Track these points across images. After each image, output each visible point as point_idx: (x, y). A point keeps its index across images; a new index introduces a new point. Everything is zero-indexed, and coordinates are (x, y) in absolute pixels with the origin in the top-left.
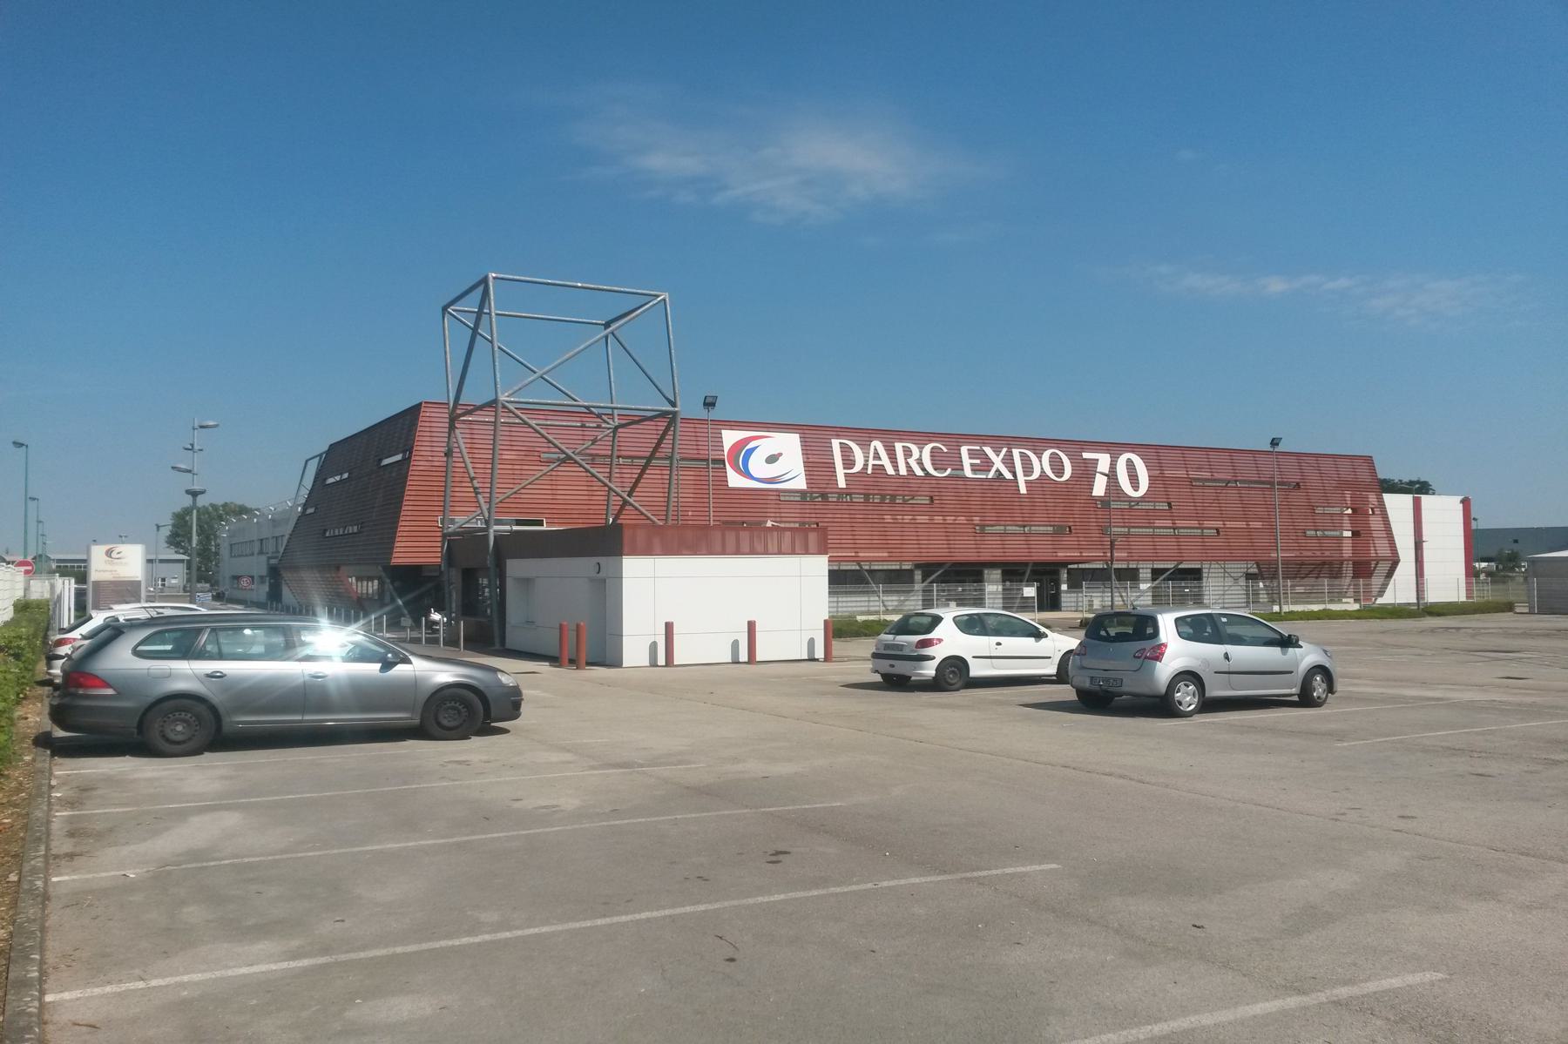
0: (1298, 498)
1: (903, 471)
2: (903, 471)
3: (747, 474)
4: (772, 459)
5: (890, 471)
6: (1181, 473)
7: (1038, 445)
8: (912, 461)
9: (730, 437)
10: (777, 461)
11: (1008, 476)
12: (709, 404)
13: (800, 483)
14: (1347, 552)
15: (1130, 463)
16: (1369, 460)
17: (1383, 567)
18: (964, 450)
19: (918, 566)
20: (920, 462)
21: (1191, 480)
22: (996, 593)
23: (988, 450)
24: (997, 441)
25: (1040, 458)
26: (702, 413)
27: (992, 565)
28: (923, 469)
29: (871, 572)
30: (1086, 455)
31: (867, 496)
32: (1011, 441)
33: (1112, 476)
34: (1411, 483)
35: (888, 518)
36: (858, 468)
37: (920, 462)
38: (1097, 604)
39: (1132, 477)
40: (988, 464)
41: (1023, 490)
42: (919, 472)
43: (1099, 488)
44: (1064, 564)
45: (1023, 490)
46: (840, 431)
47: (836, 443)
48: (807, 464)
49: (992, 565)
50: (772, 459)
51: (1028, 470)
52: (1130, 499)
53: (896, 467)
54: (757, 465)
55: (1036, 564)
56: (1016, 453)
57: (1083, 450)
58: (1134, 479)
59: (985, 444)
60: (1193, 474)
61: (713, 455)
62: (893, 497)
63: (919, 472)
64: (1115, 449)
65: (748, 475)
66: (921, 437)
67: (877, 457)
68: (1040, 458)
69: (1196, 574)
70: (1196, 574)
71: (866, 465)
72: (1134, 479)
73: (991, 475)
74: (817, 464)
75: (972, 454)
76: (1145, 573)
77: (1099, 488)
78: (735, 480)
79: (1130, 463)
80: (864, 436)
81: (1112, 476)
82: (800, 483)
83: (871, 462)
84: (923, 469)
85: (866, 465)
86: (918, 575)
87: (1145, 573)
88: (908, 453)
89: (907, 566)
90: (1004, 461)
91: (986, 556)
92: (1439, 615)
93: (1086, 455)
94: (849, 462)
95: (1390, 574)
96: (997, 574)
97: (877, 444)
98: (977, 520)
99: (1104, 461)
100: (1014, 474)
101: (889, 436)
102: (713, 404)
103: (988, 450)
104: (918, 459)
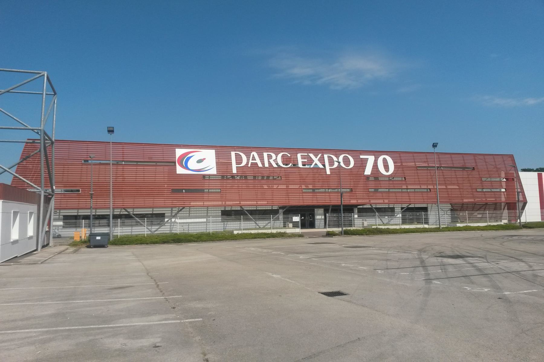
0: (475, 173)
1: (267, 165)
2: (267, 165)
3: (187, 168)
4: (200, 161)
5: (260, 165)
6: (412, 164)
7: (337, 153)
8: (272, 161)
9: (179, 152)
10: (203, 161)
11: (321, 166)
12: (435, 145)
13: (214, 171)
14: (503, 199)
15: (385, 161)
16: (511, 157)
17: (521, 205)
18: (299, 156)
19: (280, 208)
20: (275, 160)
21: (417, 168)
22: (321, 219)
23: (312, 155)
24: (316, 151)
25: (338, 158)
26: (432, 150)
27: (319, 207)
28: (277, 164)
29: (376, 208)
30: (362, 157)
31: (255, 177)
32: (324, 151)
33: (375, 166)
34: (540, 168)
35: (265, 187)
36: (244, 164)
37: (275, 160)
38: (366, 224)
39: (387, 166)
40: (311, 161)
41: (328, 172)
42: (275, 166)
43: (368, 171)
44: (356, 206)
45: (328, 172)
46: (234, 148)
47: (233, 154)
48: (217, 163)
49: (319, 207)
50: (200, 161)
51: (331, 162)
52: (389, 176)
53: (263, 164)
54: (193, 164)
55: (333, 206)
56: (326, 156)
57: (361, 154)
58: (386, 167)
59: (310, 153)
60: (418, 164)
61: (171, 160)
62: (268, 177)
63: (275, 166)
64: (377, 154)
65: (187, 168)
66: (277, 150)
67: (254, 159)
68: (338, 158)
69: (425, 209)
70: (425, 209)
71: (248, 163)
72: (386, 167)
73: (312, 166)
74: (223, 164)
75: (303, 157)
76: (398, 209)
77: (368, 171)
78: (180, 170)
79: (385, 161)
80: (247, 150)
81: (375, 166)
82: (214, 171)
83: (251, 161)
84: (277, 164)
85: (248, 163)
86: (281, 211)
87: (398, 209)
88: (270, 157)
89: (275, 208)
90: (319, 160)
91: (315, 203)
92: (530, 228)
93: (362, 157)
94: (239, 160)
95: (523, 208)
96: (321, 211)
97: (255, 154)
98: (310, 187)
99: (371, 159)
100: (324, 165)
101: (260, 150)
102: (436, 146)
103: (312, 155)
104: (277, 160)
